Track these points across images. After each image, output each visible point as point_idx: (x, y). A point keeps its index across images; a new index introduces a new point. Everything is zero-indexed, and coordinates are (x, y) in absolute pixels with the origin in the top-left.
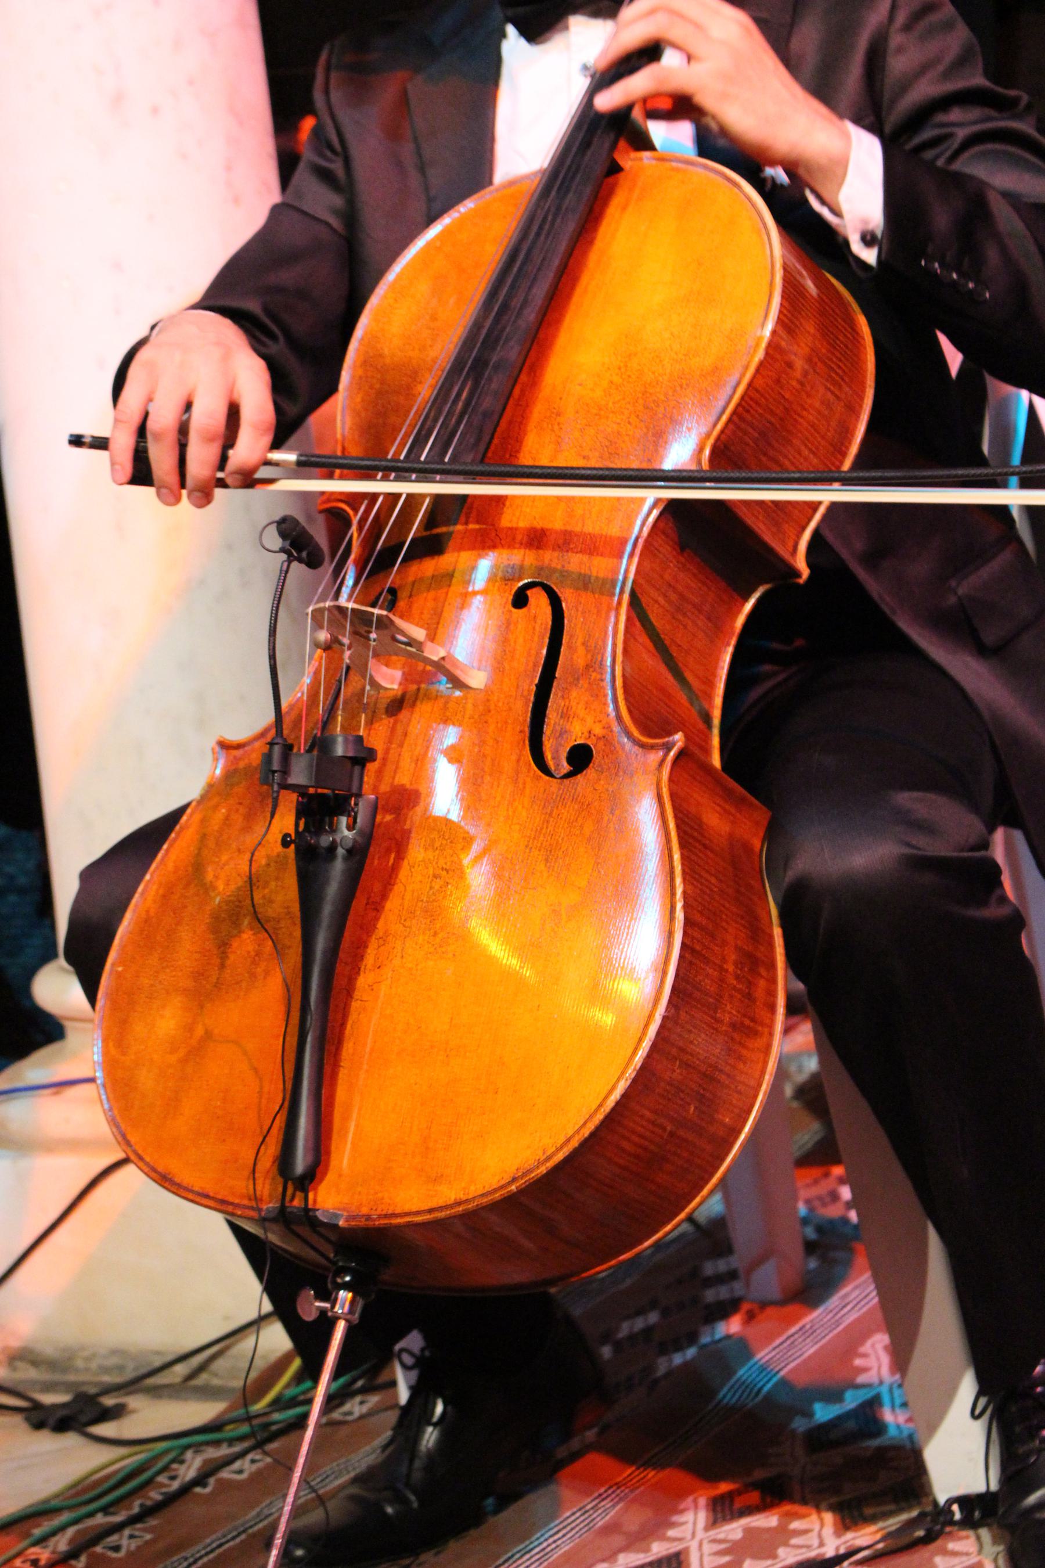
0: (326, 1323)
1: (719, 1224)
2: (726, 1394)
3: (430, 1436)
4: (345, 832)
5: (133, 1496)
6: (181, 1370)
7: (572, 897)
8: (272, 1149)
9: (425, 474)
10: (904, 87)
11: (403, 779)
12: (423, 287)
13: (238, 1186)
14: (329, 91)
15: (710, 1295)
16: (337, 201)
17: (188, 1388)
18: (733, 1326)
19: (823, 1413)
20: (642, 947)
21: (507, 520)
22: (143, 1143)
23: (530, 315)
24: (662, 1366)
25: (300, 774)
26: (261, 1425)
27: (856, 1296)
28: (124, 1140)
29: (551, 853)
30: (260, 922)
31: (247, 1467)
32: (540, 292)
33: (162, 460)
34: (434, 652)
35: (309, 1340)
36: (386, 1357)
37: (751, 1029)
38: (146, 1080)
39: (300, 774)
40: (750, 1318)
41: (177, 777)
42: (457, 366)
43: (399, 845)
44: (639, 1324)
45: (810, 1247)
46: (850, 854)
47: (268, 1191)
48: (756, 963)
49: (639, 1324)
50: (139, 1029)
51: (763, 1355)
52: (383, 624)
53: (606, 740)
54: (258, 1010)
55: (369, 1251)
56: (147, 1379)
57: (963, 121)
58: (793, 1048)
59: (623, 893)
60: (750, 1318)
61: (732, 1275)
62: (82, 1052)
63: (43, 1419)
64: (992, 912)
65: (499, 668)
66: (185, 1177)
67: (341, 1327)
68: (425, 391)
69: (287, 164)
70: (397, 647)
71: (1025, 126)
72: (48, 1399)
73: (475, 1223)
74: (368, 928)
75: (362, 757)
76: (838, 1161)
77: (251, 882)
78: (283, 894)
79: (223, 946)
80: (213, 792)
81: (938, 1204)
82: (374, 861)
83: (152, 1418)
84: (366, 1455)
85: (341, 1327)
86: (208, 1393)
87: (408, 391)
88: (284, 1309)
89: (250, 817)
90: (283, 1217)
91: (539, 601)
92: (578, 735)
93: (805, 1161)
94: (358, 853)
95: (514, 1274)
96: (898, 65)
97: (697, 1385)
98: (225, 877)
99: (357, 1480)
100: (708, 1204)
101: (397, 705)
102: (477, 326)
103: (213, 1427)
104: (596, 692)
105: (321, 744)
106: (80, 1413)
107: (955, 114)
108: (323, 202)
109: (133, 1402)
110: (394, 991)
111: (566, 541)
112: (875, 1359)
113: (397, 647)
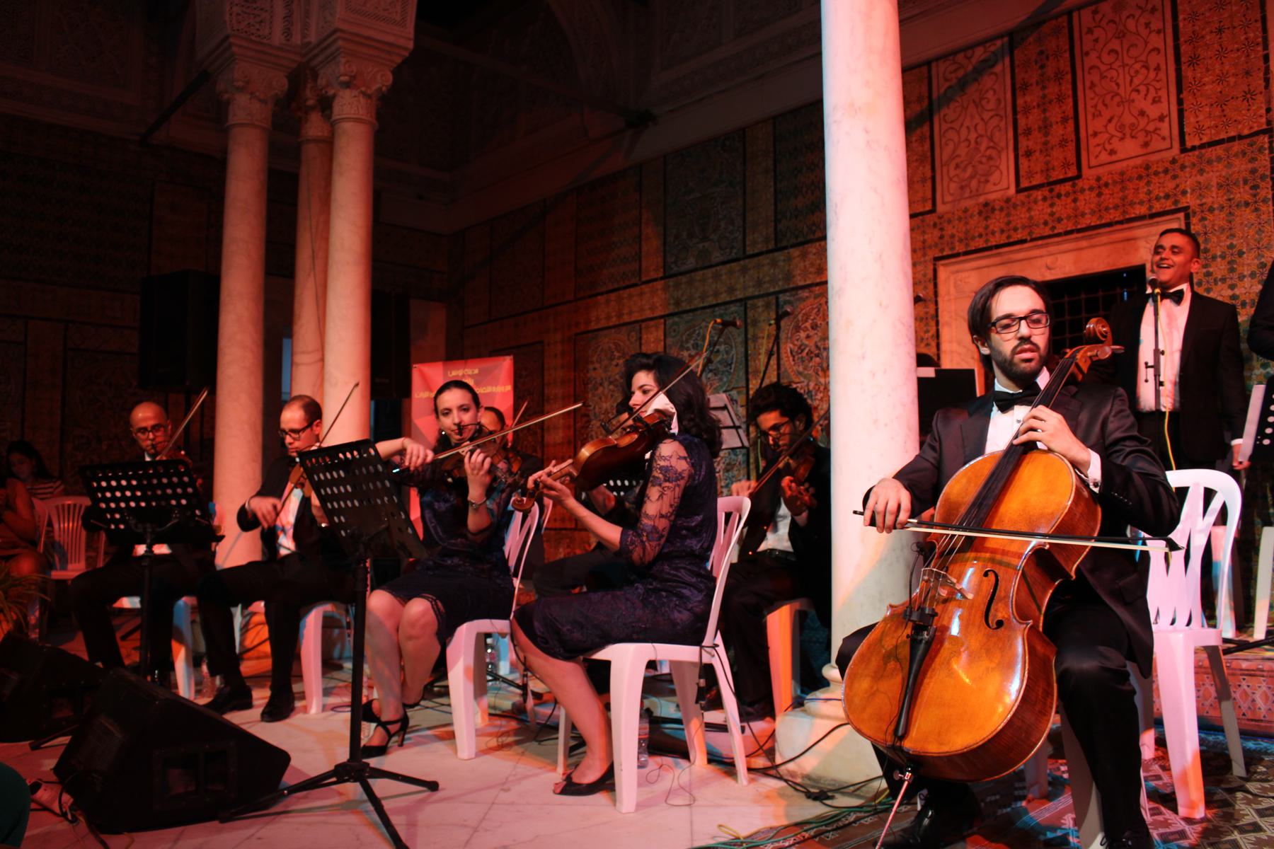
0: (902, 781)
1: (1022, 771)
2: (1019, 824)
3: (926, 821)
4: (925, 636)
5: (835, 824)
6: (852, 788)
7: (993, 665)
8: (892, 727)
9: (965, 530)
10: (1112, 433)
11: (945, 623)
12: (964, 481)
13: (880, 736)
14: (937, 422)
15: (1016, 793)
16: (935, 455)
17: (853, 794)
18: (1024, 803)
19: (1050, 835)
20: (1015, 686)
21: (988, 545)
22: (853, 719)
23: (997, 492)
24: (999, 812)
25: (914, 618)
26: (877, 808)
27: (1066, 800)
28: (848, 716)
29: (988, 652)
30: (897, 659)
31: (869, 820)
32: (1000, 485)
33: (879, 519)
34: (958, 587)
35: (894, 786)
36: (915, 796)
37: (1045, 714)
38: (857, 701)
39: (914, 618)
40: (1029, 802)
41: (873, 614)
42: (973, 505)
43: (942, 643)
44: (993, 798)
45: (1050, 784)
46: (1084, 663)
47: (890, 740)
48: (1049, 693)
49: (993, 798)
50: (856, 685)
51: (1032, 814)
52: (944, 576)
53: (1008, 619)
54: (893, 685)
55: (918, 762)
56: (842, 789)
57: (1130, 446)
58: (1054, 721)
59: (1008, 667)
60: (1029, 802)
61: (1024, 788)
62: (837, 691)
63: (809, 795)
64: (1126, 688)
65: (977, 594)
66: (865, 731)
67: (906, 784)
68: (963, 510)
69: (921, 444)
70: (946, 583)
71: (1149, 450)
72: (812, 790)
73: (951, 759)
74: (929, 666)
75: (934, 614)
76: (1063, 758)
77: (896, 647)
78: (905, 652)
79: (886, 664)
80: (886, 620)
81: (1098, 777)
82: (933, 646)
83: (842, 801)
84: (906, 823)
85: (906, 784)
86: (859, 797)
87: (957, 510)
88: (887, 774)
89: (897, 628)
90: (893, 748)
91: (992, 577)
92: (1000, 616)
93: (1051, 757)
94: (929, 643)
95: (958, 776)
96: (1111, 426)
97: (1010, 820)
98: (889, 644)
99: (903, 830)
100: (1020, 766)
101: (946, 601)
102: (980, 493)
103: (860, 807)
104: (1006, 605)
105: (921, 609)
106: (821, 796)
107: (1127, 443)
108: (931, 455)
109: (837, 795)
110: (932, 687)
111: (1004, 553)
112: (1068, 821)
113: (946, 583)
